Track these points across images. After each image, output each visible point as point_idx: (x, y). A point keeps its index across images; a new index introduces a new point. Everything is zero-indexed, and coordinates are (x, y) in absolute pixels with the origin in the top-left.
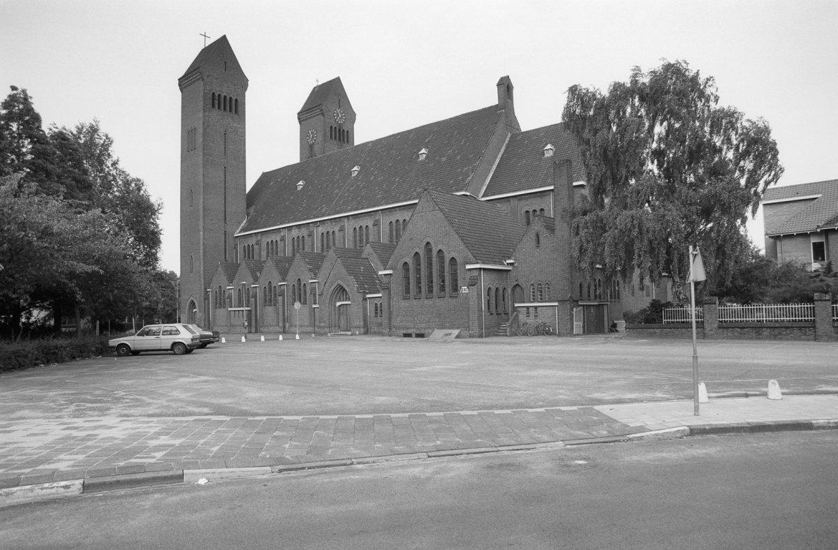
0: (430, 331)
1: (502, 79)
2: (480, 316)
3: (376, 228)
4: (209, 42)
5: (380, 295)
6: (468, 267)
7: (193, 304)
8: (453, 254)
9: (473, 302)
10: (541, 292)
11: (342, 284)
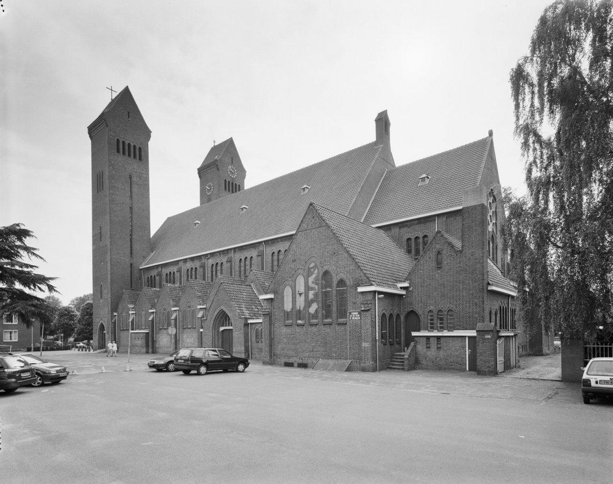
0: (315, 362)
1: (380, 114)
2: (374, 346)
3: (260, 258)
4: (115, 95)
5: (261, 321)
6: (360, 289)
7: (102, 327)
8: (342, 276)
9: (367, 329)
10: (441, 319)
11: (225, 309)
